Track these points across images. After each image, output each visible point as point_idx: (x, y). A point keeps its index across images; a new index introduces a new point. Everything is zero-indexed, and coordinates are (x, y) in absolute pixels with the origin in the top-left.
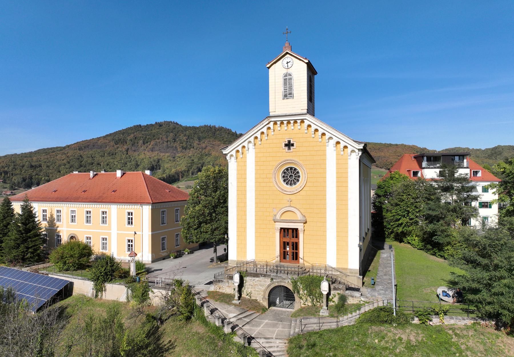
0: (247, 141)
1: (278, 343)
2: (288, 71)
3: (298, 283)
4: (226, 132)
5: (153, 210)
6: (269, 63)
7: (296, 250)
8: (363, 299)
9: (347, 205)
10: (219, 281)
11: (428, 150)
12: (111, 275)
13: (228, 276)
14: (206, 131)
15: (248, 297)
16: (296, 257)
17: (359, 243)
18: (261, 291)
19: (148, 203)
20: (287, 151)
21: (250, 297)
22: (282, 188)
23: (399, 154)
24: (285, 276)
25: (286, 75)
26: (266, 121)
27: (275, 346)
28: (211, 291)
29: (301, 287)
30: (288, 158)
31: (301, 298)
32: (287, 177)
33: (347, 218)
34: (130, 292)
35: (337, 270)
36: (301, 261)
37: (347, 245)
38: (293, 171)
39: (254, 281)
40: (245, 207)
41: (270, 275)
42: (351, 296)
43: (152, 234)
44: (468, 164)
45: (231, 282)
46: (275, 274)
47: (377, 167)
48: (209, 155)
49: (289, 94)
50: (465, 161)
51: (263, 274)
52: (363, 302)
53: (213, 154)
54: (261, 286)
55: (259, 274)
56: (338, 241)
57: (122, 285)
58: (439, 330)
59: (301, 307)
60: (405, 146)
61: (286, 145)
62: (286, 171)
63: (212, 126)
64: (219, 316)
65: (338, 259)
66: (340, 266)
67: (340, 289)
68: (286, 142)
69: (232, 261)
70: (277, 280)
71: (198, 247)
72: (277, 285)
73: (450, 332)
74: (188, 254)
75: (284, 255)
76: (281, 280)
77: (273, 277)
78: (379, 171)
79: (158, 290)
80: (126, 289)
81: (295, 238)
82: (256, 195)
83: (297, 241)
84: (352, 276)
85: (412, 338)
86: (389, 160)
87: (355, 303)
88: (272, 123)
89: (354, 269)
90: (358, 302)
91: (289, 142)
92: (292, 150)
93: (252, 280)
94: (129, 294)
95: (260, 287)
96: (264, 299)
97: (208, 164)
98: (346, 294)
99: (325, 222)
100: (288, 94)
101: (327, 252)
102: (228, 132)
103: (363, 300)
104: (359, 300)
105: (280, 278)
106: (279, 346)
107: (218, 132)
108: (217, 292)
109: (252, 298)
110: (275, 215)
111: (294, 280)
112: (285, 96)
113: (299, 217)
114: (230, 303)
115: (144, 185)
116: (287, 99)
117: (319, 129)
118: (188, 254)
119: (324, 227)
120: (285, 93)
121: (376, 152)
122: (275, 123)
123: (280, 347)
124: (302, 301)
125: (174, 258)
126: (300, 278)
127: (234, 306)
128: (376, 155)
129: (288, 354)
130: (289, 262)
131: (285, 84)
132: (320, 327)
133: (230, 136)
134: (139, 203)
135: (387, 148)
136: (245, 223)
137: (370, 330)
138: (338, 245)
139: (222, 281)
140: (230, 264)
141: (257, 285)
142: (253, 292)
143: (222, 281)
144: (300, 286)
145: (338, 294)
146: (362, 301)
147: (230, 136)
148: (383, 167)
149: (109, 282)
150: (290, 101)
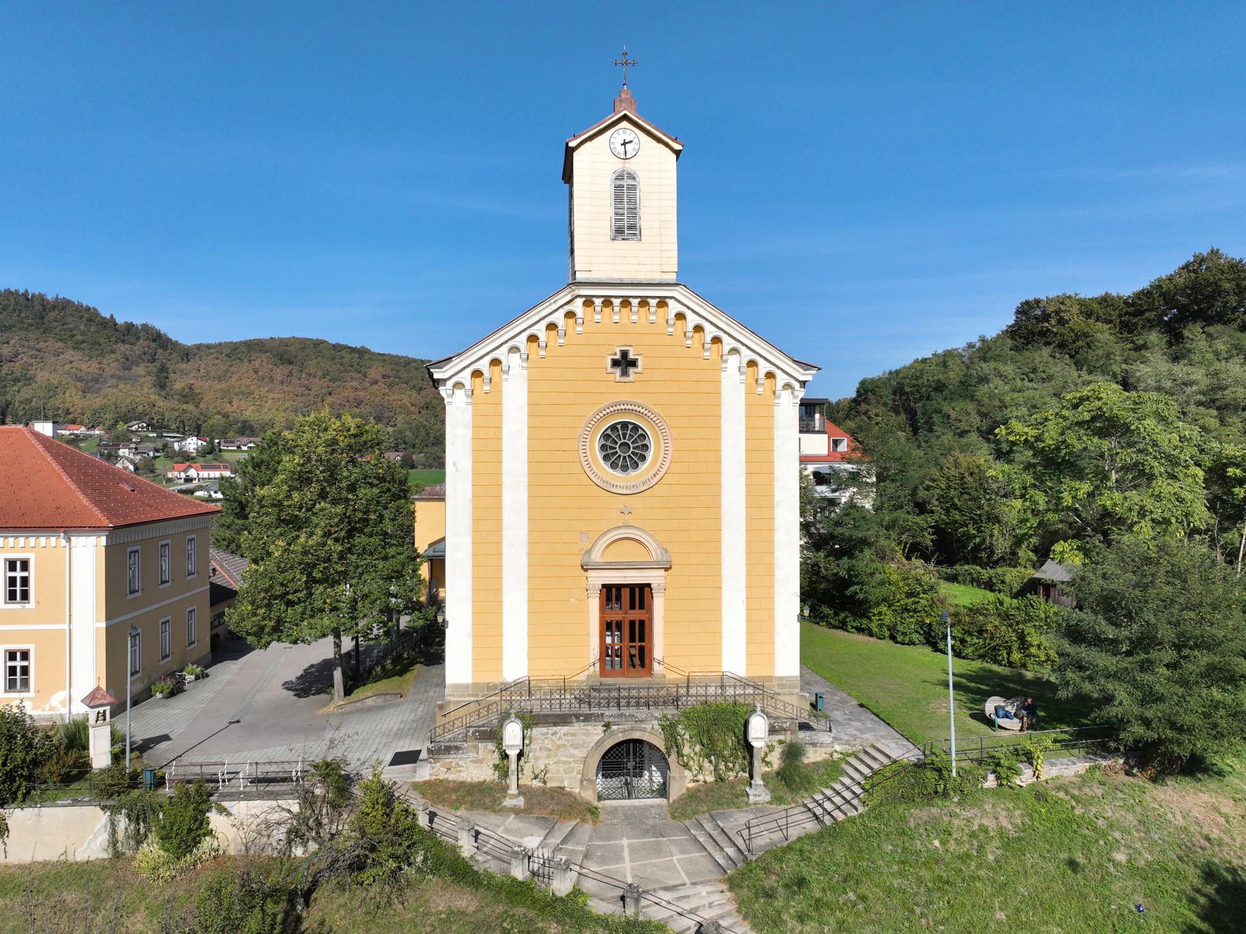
0: (506, 347)
1: (704, 894)
2: (627, 165)
3: (680, 729)
4: (82, 317)
5: (111, 552)
6: (575, 137)
8: (838, 748)
9: (771, 519)
10: (448, 750)
12: (29, 778)
13: (476, 731)
14: (11, 307)
15: (536, 784)
16: (641, 659)
17: (798, 612)
18: (576, 762)
19: (94, 529)
21: (545, 783)
22: (607, 479)
24: (642, 713)
25: (619, 176)
26: (565, 296)
27: (704, 906)
28: (421, 780)
29: (687, 736)
31: (686, 766)
32: (612, 448)
33: (771, 551)
34: (123, 822)
35: (744, 683)
36: (657, 668)
37: (771, 619)
38: (629, 432)
39: (554, 737)
40: (498, 530)
41: (602, 714)
42: (809, 744)
43: (107, 628)
44: (823, 424)
45: (485, 748)
48: (28, 379)
49: (630, 228)
50: (817, 416)
51: (581, 715)
52: (840, 756)
53: (38, 379)
54: (576, 748)
55: (570, 716)
56: (749, 611)
57: (89, 803)
58: (1039, 795)
59: (688, 789)
61: (615, 363)
62: (609, 432)
63: (33, 295)
64: (524, 850)
66: (756, 673)
67: (785, 730)
68: (615, 354)
69: (457, 687)
70: (622, 727)
71: (210, 655)
72: (621, 739)
73: (1061, 795)
74: (197, 678)
76: (634, 725)
77: (611, 720)
79: (274, 803)
80: (103, 818)
84: (784, 694)
85: (1004, 822)
87: (819, 759)
88: (580, 301)
90: (827, 756)
91: (624, 354)
92: (632, 377)
93: (548, 733)
94: (121, 835)
95: (571, 751)
96: (585, 783)
97: (22, 406)
98: (799, 741)
99: (719, 564)
100: (626, 229)
101: (723, 640)
102: (87, 315)
103: (838, 750)
104: (829, 750)
106: (713, 903)
107: (53, 314)
108: (441, 781)
109: (549, 785)
110: (589, 552)
111: (668, 720)
112: (619, 232)
113: (655, 554)
114: (497, 808)
115: (54, 470)
116: (623, 239)
117: (706, 325)
118: (197, 678)
119: (717, 575)
120: (619, 224)
122: (588, 302)
123: (715, 903)
124: (687, 773)
125: (168, 698)
126: (685, 712)
127: (513, 816)
129: (745, 918)
130: (623, 675)
131: (618, 198)
132: (785, 832)
133: (93, 329)
134: (63, 529)
137: (912, 820)
138: (749, 620)
139: (457, 748)
140: (450, 695)
141: (564, 746)
142: (553, 768)
143: (457, 748)
144: (684, 733)
145: (781, 742)
146: (836, 751)
147: (93, 329)
149: (24, 801)
150: (631, 244)
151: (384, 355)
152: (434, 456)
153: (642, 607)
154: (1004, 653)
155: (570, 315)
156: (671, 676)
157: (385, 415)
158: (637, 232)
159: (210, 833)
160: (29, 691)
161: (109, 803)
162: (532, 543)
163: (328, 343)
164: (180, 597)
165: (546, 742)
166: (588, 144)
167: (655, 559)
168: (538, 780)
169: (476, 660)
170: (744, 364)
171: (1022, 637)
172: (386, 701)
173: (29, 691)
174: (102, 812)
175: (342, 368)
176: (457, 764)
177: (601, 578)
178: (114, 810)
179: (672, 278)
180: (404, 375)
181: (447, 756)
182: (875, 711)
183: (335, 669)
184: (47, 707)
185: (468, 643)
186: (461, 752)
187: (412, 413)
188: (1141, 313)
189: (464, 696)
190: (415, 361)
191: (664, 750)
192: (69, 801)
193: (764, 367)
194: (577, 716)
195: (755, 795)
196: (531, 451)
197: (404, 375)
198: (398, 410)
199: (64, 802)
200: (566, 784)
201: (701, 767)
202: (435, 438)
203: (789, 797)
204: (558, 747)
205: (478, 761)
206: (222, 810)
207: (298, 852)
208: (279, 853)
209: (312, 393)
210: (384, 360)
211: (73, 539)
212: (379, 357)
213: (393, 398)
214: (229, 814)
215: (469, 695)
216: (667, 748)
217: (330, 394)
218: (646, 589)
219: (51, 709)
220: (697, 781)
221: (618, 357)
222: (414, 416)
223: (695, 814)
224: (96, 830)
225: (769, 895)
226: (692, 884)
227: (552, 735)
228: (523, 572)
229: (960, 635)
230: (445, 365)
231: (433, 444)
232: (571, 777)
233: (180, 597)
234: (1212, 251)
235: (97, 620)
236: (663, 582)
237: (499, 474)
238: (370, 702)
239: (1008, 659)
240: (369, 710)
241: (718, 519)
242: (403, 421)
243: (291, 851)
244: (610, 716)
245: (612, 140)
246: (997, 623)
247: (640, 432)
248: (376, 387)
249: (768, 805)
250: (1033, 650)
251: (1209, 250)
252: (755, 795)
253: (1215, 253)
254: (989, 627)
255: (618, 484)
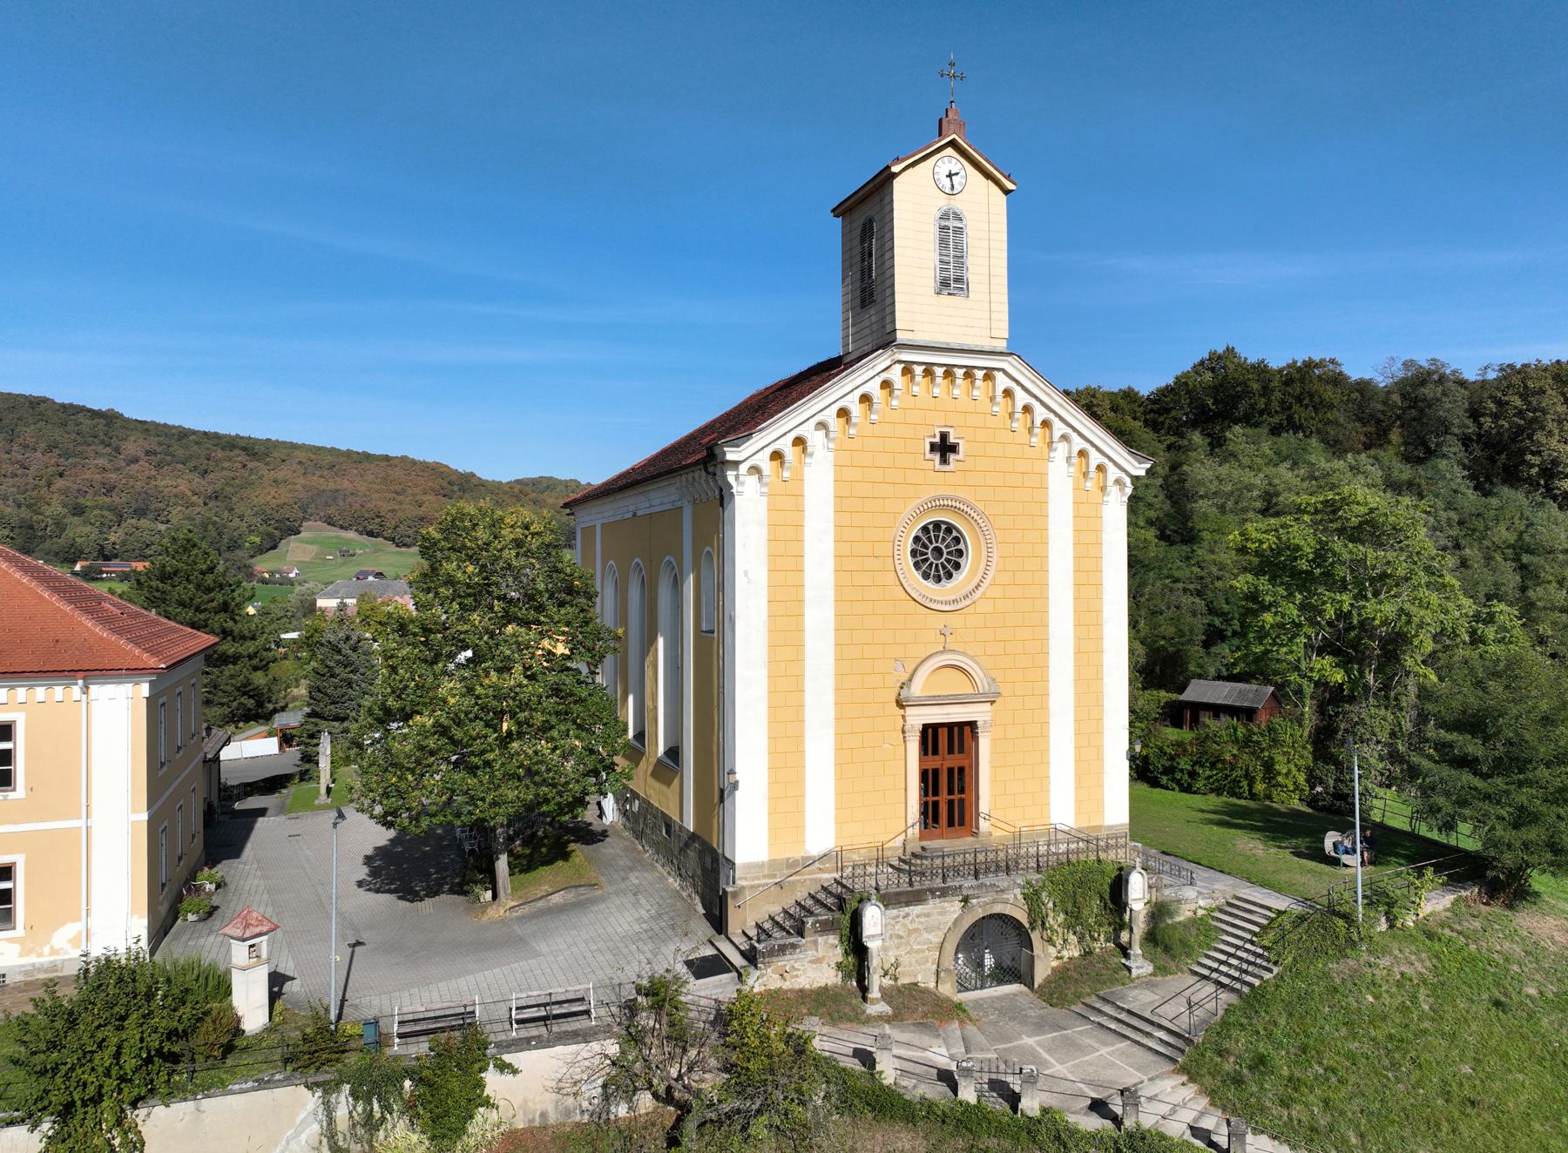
1: (1169, 1090)
7: (933, 795)
8: (1202, 903)
11: (480, 479)
17: (1127, 747)
19: (132, 672)
20: (938, 466)
23: (398, 488)
24: (1002, 880)
25: (945, 215)
26: (884, 360)
29: (1051, 905)
30: (941, 492)
31: (1050, 941)
40: (799, 659)
41: (960, 886)
45: (826, 943)
46: (971, 882)
47: (329, 524)
51: (937, 890)
52: (1204, 912)
57: (287, 1082)
60: (414, 462)
61: (953, 449)
65: (1078, 803)
68: (934, 436)
69: (749, 866)
75: (930, 815)
77: (971, 892)
78: (337, 537)
81: (957, 755)
82: (838, 615)
83: (965, 763)
86: (369, 505)
88: (899, 367)
89: (1116, 826)
90: (1191, 914)
93: (898, 917)
95: (926, 935)
100: (951, 282)
104: (1193, 907)
105: (990, 889)
112: (945, 283)
116: (949, 294)
119: (1044, 707)
120: (945, 274)
121: (321, 477)
122: (908, 370)
128: (324, 487)
131: (943, 242)
135: (359, 466)
136: (800, 720)
140: (741, 879)
141: (916, 930)
142: (904, 960)
146: (1200, 907)
148: (350, 525)
151: (145, 422)
152: (239, 564)
153: (961, 751)
154: (1245, 783)
155: (886, 384)
156: (997, 833)
157: (152, 507)
158: (965, 287)
159: (487, 1103)
160: (14, 928)
161: (321, 1078)
162: (840, 676)
163: (54, 403)
164: (180, 779)
165: (897, 927)
166: (910, 170)
167: (981, 691)
168: (888, 977)
169: (773, 830)
170: (1075, 454)
171: (1269, 767)
172: (579, 895)
173: (14, 928)
174: (308, 1093)
175: (79, 439)
176: (793, 967)
177: (919, 717)
178: (328, 1088)
179: (1002, 345)
180: (180, 453)
181: (781, 958)
182: (1190, 858)
183: (498, 859)
184: (46, 950)
185: (763, 808)
186: (798, 951)
187: (193, 505)
188: (1168, 411)
189: (758, 878)
190: (194, 433)
191: (1027, 925)
192: (250, 1084)
193: (1095, 458)
194: (932, 891)
195: (1138, 968)
196: (838, 557)
197: (180, 452)
198: (173, 500)
199: (244, 1086)
200: (919, 978)
201: (1065, 941)
202: (231, 539)
203: (1172, 965)
204: (910, 932)
205: (817, 961)
206: (504, 1067)
207: (622, 1110)
208: (591, 1116)
209: (32, 472)
210: (147, 430)
211: (93, 688)
212: (139, 425)
213: (163, 483)
214: (515, 1072)
215: (764, 877)
216: (1031, 924)
217: (61, 475)
218: (967, 729)
219: (53, 952)
220: (1061, 958)
221: (937, 440)
222: (198, 509)
223: (1078, 997)
224: (298, 1122)
225: (1238, 1081)
226: (1150, 1079)
227: (904, 918)
228: (829, 712)
229: (1189, 768)
230: (744, 443)
231: (229, 548)
232: (924, 970)
233: (180, 779)
234: (1228, 349)
235: (134, 811)
236: (989, 718)
237: (800, 586)
238: (557, 899)
239: (1250, 791)
240: (561, 909)
241: (1045, 640)
242: (181, 516)
243: (608, 1112)
244: (969, 888)
245: (936, 169)
246: (1235, 752)
247: (955, 534)
248: (135, 467)
249: (1153, 978)
250: (1280, 779)
251: (1225, 348)
252: (1138, 968)
253: (1230, 351)
254: (1228, 757)
255: (937, 598)
